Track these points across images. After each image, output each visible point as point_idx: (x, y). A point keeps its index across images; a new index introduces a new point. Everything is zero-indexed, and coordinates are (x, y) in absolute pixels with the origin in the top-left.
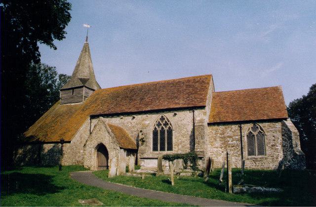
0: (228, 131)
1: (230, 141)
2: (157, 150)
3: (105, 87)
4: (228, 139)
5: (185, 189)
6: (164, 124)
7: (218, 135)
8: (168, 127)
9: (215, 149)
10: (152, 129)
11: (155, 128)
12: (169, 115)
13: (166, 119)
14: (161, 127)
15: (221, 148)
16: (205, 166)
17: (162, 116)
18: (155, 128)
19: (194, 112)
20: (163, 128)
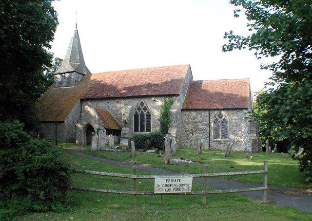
7: (190, 120)
11: (136, 112)
20: (142, 112)
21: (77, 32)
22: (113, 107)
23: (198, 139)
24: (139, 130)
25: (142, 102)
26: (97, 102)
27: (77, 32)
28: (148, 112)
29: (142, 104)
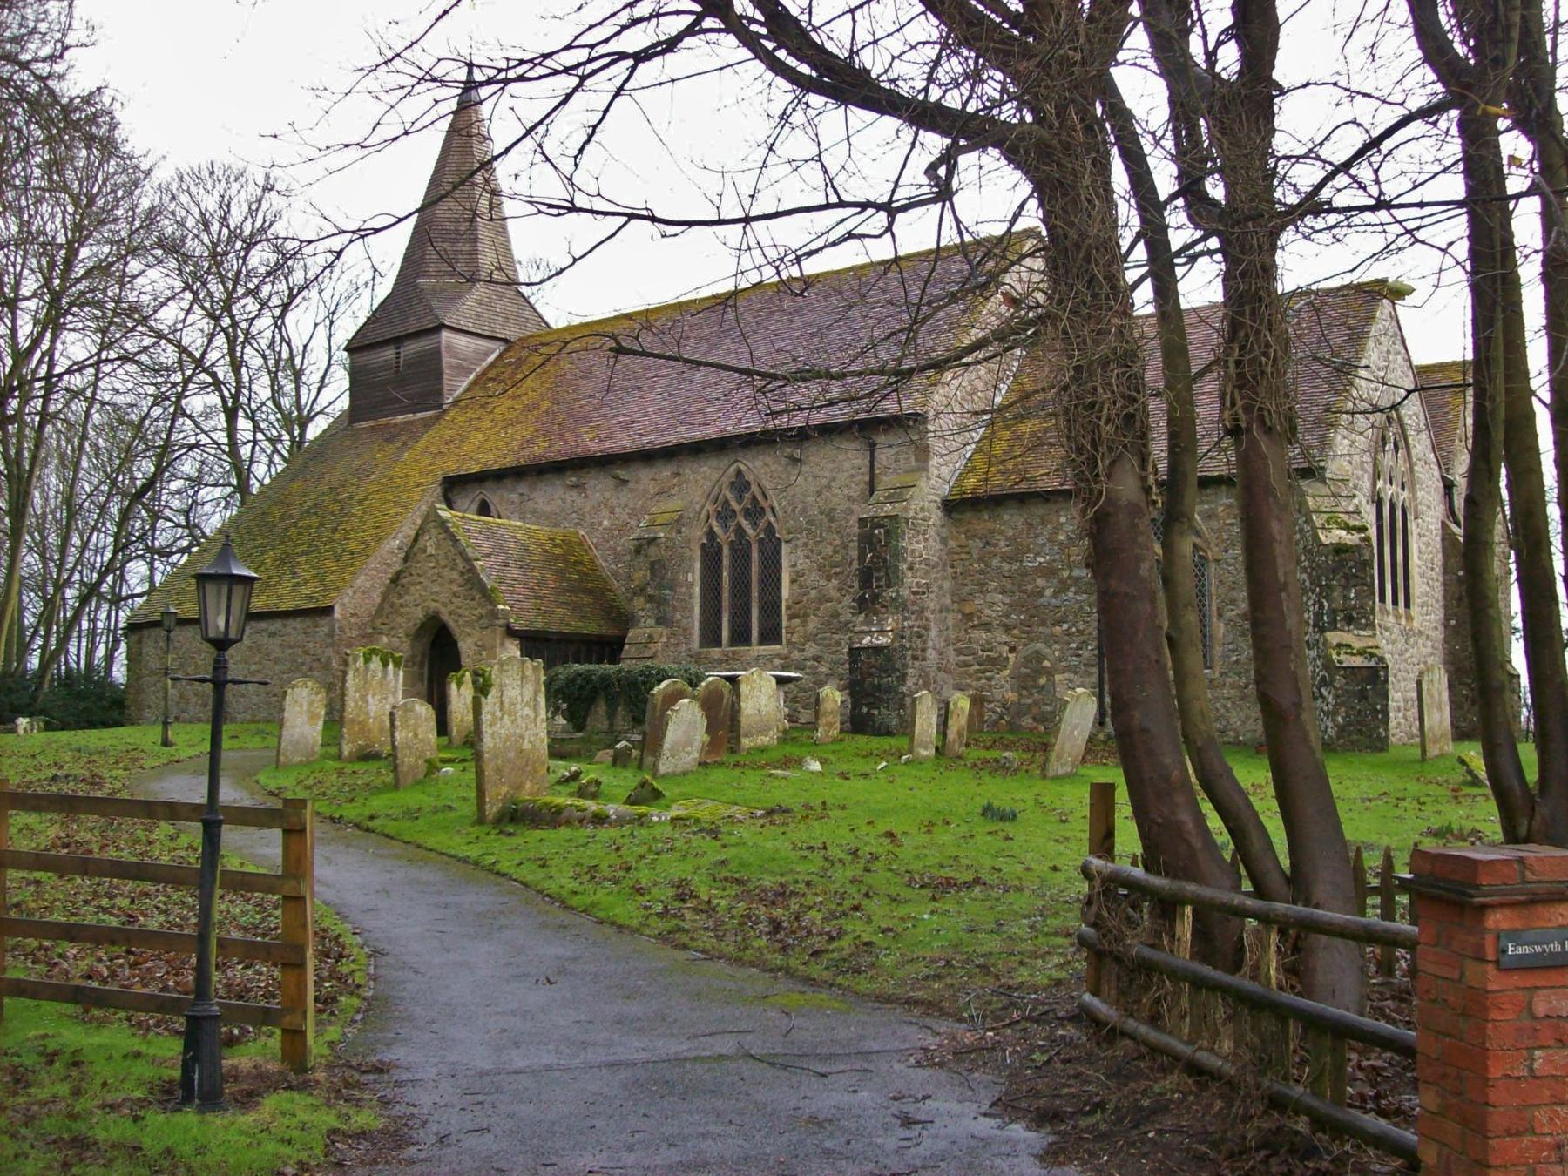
0: (1040, 540)
1: (1049, 592)
2: (718, 643)
3: (562, 324)
4: (1040, 582)
5: (392, 605)
6: (747, 513)
7: (995, 562)
8: (762, 524)
9: (981, 635)
10: (698, 534)
11: (711, 534)
12: (761, 468)
13: (754, 488)
14: (732, 525)
15: (1007, 629)
16: (1379, 863)
17: (739, 473)
18: (711, 534)
19: (873, 446)
20: (740, 530)
23: (1041, 671)
24: (725, 634)
25: (739, 473)
26: (523, 487)
28: (770, 529)
29: (740, 485)
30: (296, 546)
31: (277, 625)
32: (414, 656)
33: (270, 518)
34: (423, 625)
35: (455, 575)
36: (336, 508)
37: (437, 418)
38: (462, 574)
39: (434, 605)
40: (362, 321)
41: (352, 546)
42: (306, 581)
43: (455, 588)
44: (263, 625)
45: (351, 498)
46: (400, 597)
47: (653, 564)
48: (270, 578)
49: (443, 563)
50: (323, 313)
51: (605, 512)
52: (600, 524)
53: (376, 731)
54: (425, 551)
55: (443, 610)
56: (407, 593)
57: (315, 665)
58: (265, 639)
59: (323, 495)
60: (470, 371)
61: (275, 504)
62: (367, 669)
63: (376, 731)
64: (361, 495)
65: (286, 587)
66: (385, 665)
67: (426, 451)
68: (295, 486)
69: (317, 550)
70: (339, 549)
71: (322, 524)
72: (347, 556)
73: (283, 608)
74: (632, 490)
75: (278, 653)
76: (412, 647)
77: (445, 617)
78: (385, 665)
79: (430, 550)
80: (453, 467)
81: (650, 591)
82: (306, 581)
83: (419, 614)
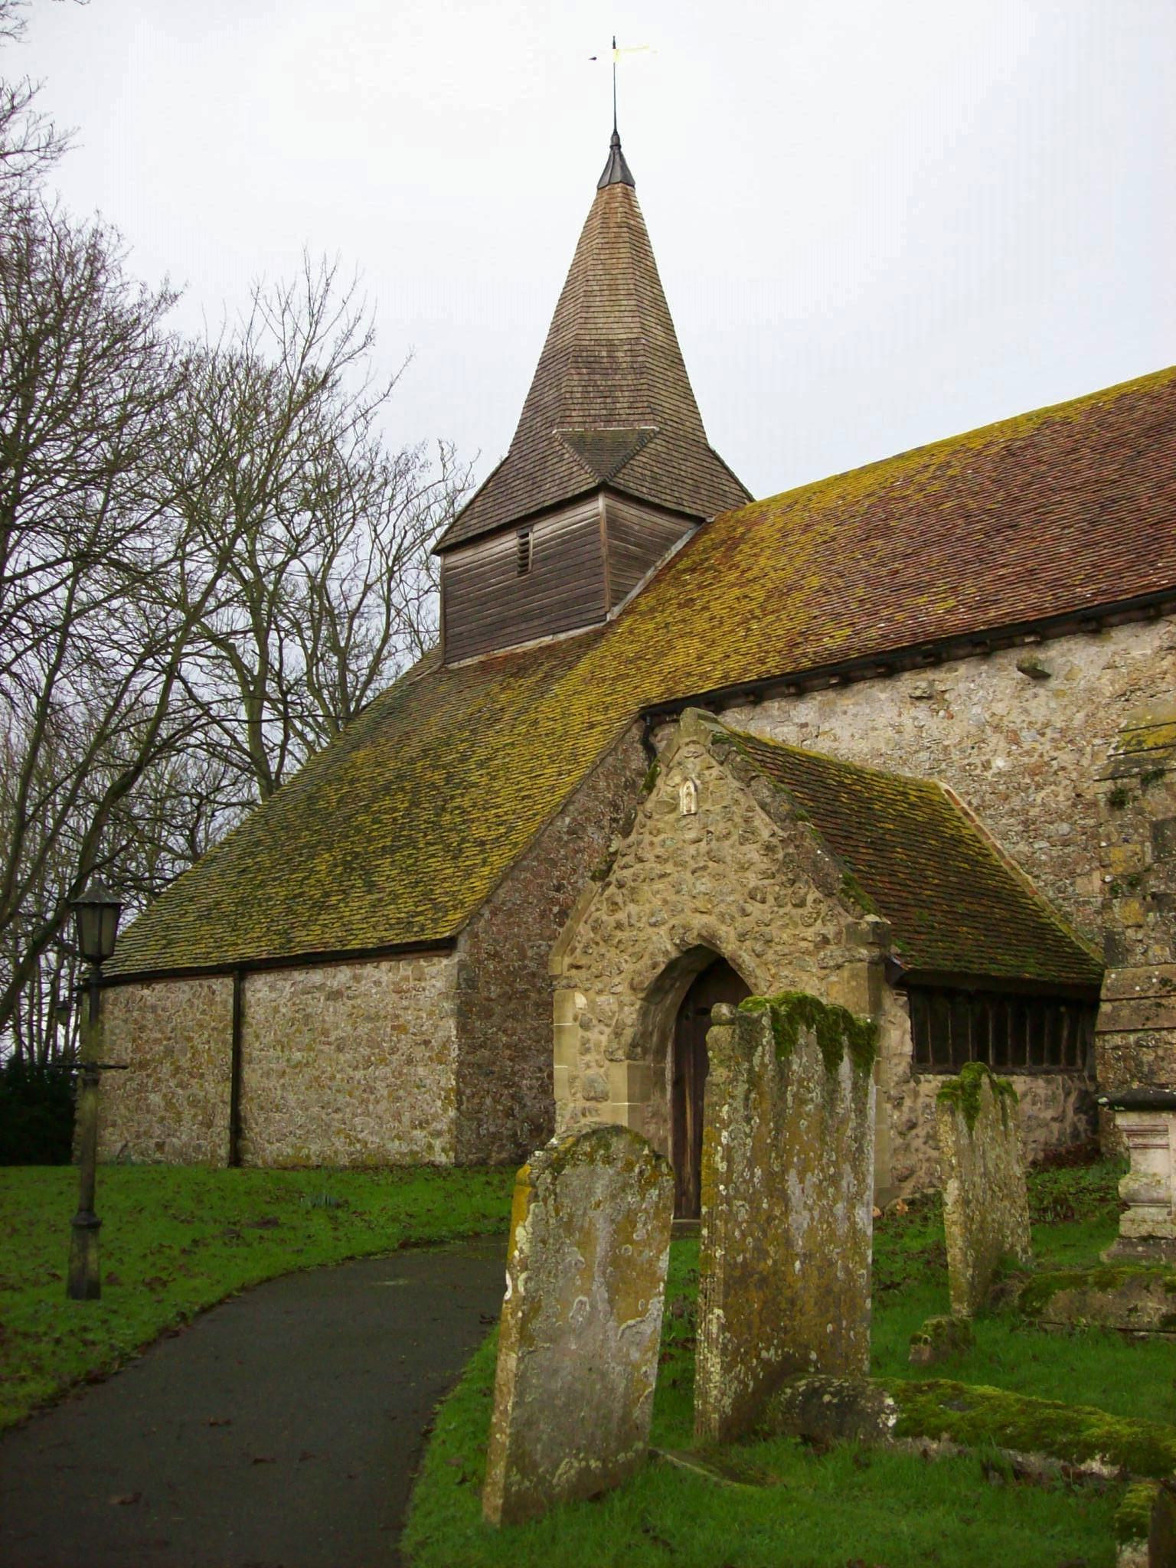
21: (615, 132)
22: (980, 743)
27: (615, 132)
30: (370, 841)
31: (342, 975)
32: (645, 1035)
33: (322, 804)
34: (672, 966)
35: (752, 853)
36: (438, 777)
37: (599, 635)
38: (769, 849)
39: (698, 921)
40: (41, 1168)
41: (479, 831)
42: (395, 897)
43: (752, 880)
44: (317, 976)
45: (464, 759)
46: (614, 906)
47: (1157, 828)
48: (327, 895)
49: (720, 828)
50: (379, 565)
51: (996, 740)
52: (987, 766)
53: (809, 1300)
54: (674, 808)
55: (723, 930)
56: (633, 896)
57: (420, 1052)
58: (318, 1004)
59: (412, 761)
60: (647, 565)
61: (330, 783)
62: (783, 1076)
63: (809, 1300)
64: (482, 753)
65: (357, 907)
66: (832, 1061)
67: (591, 679)
68: (360, 756)
69: (412, 843)
70: (454, 839)
71: (414, 804)
72: (470, 849)
73: (355, 945)
74: (1057, 694)
75: (345, 1029)
76: (644, 1013)
77: (729, 947)
78: (832, 1061)
79: (686, 804)
80: (654, 691)
81: (1155, 885)
82: (395, 897)
83: (663, 945)
